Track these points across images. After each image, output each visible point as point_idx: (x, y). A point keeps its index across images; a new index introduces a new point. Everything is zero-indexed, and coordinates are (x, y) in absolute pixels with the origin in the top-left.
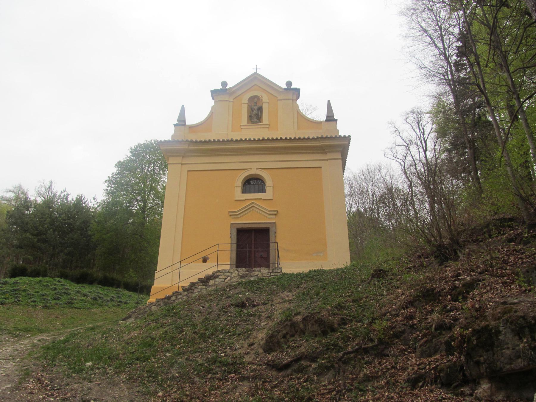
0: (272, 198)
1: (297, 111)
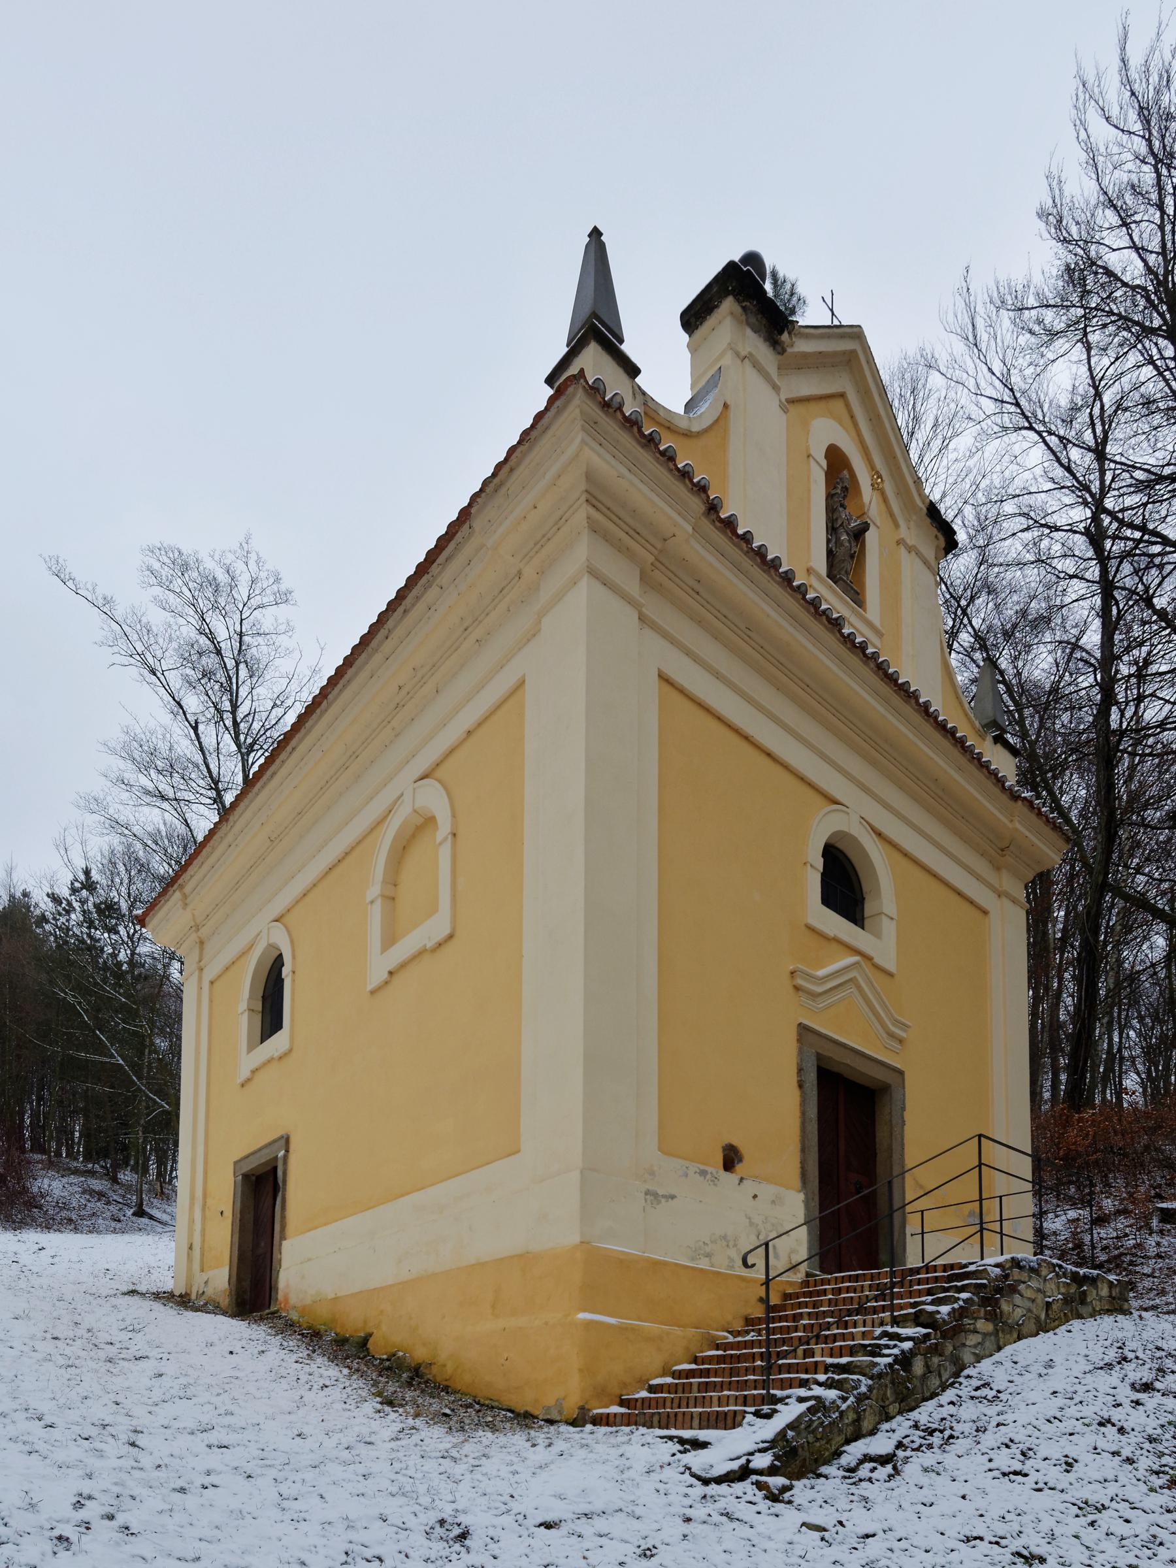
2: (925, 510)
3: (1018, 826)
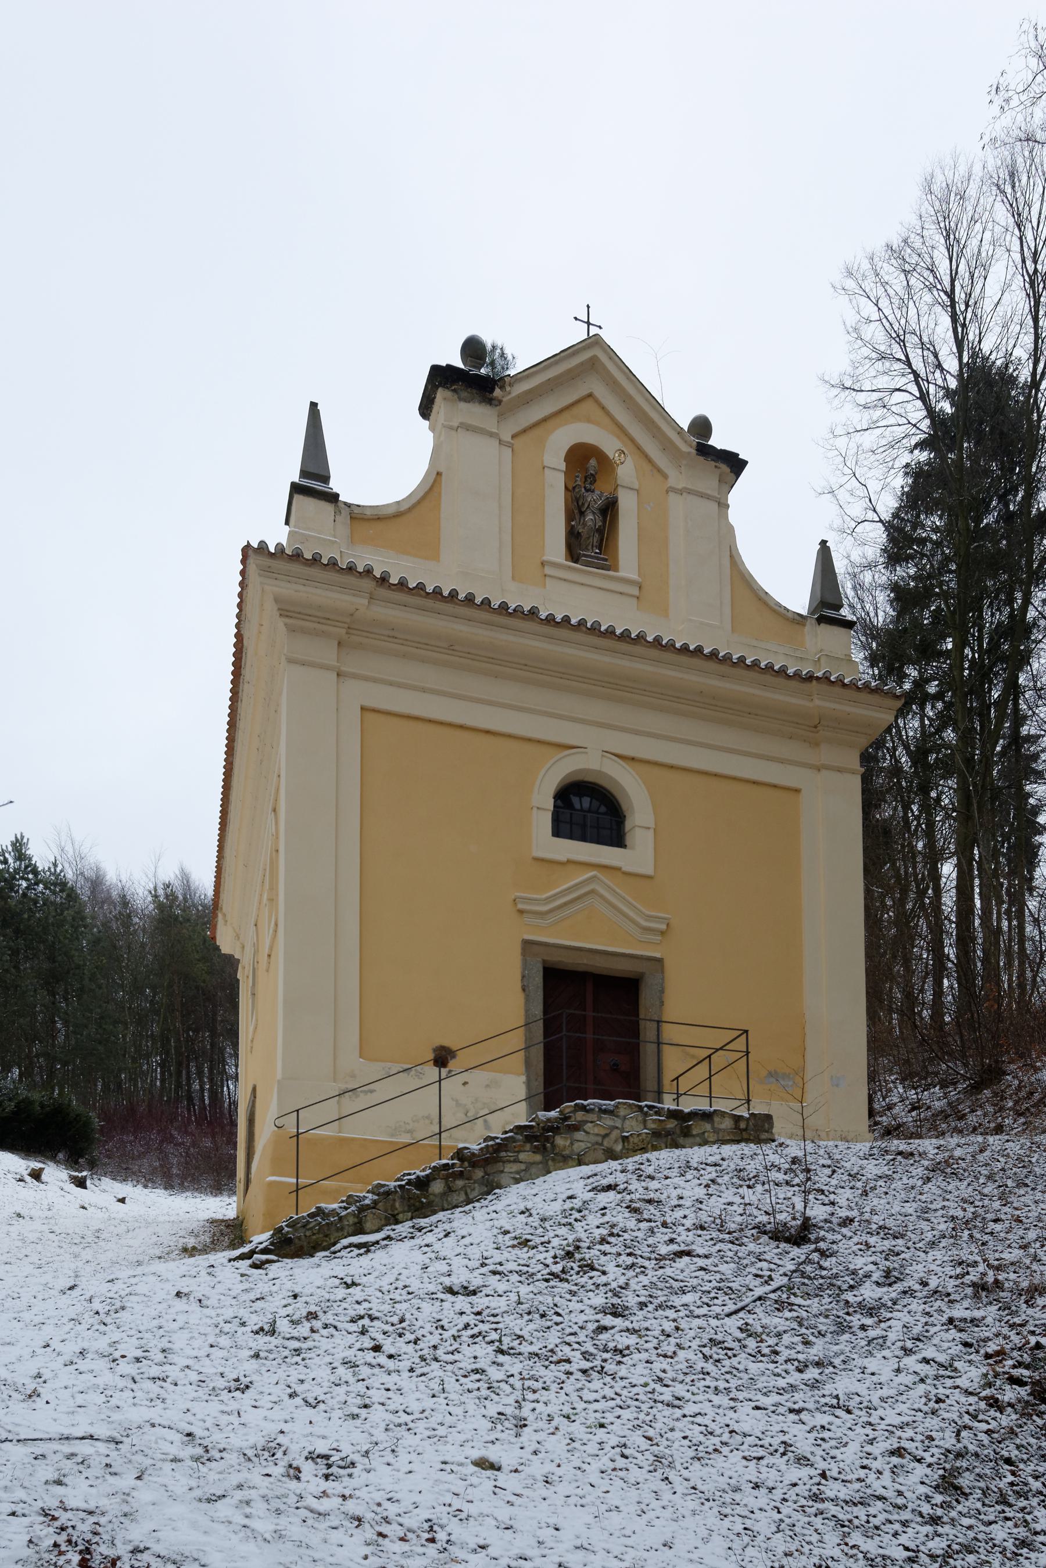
0: (649, 870)
1: (731, 556)
2: (694, 452)
3: (817, 702)
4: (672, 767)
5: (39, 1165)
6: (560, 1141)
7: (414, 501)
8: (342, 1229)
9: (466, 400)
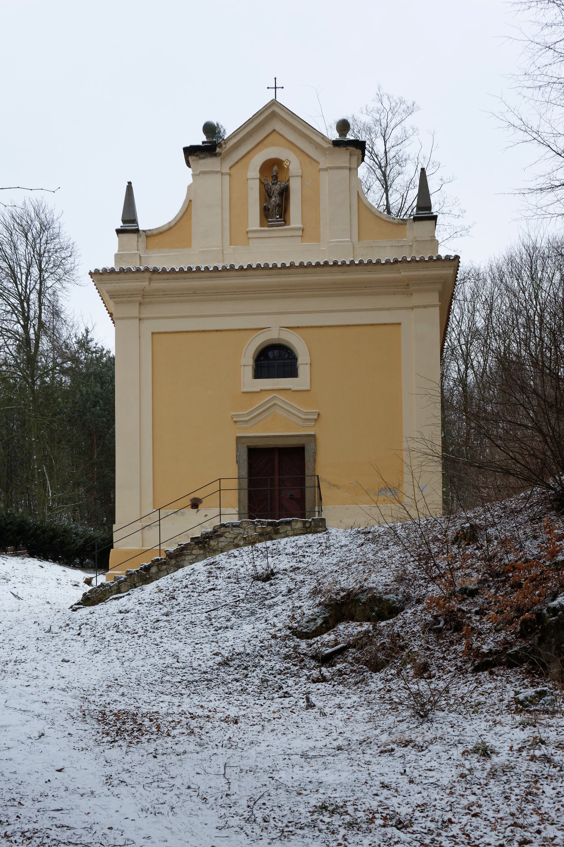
0: (308, 388)
4: (321, 327)
5: (89, 576)
6: (212, 543)
7: (177, 219)
8: (111, 592)
9: (203, 158)
